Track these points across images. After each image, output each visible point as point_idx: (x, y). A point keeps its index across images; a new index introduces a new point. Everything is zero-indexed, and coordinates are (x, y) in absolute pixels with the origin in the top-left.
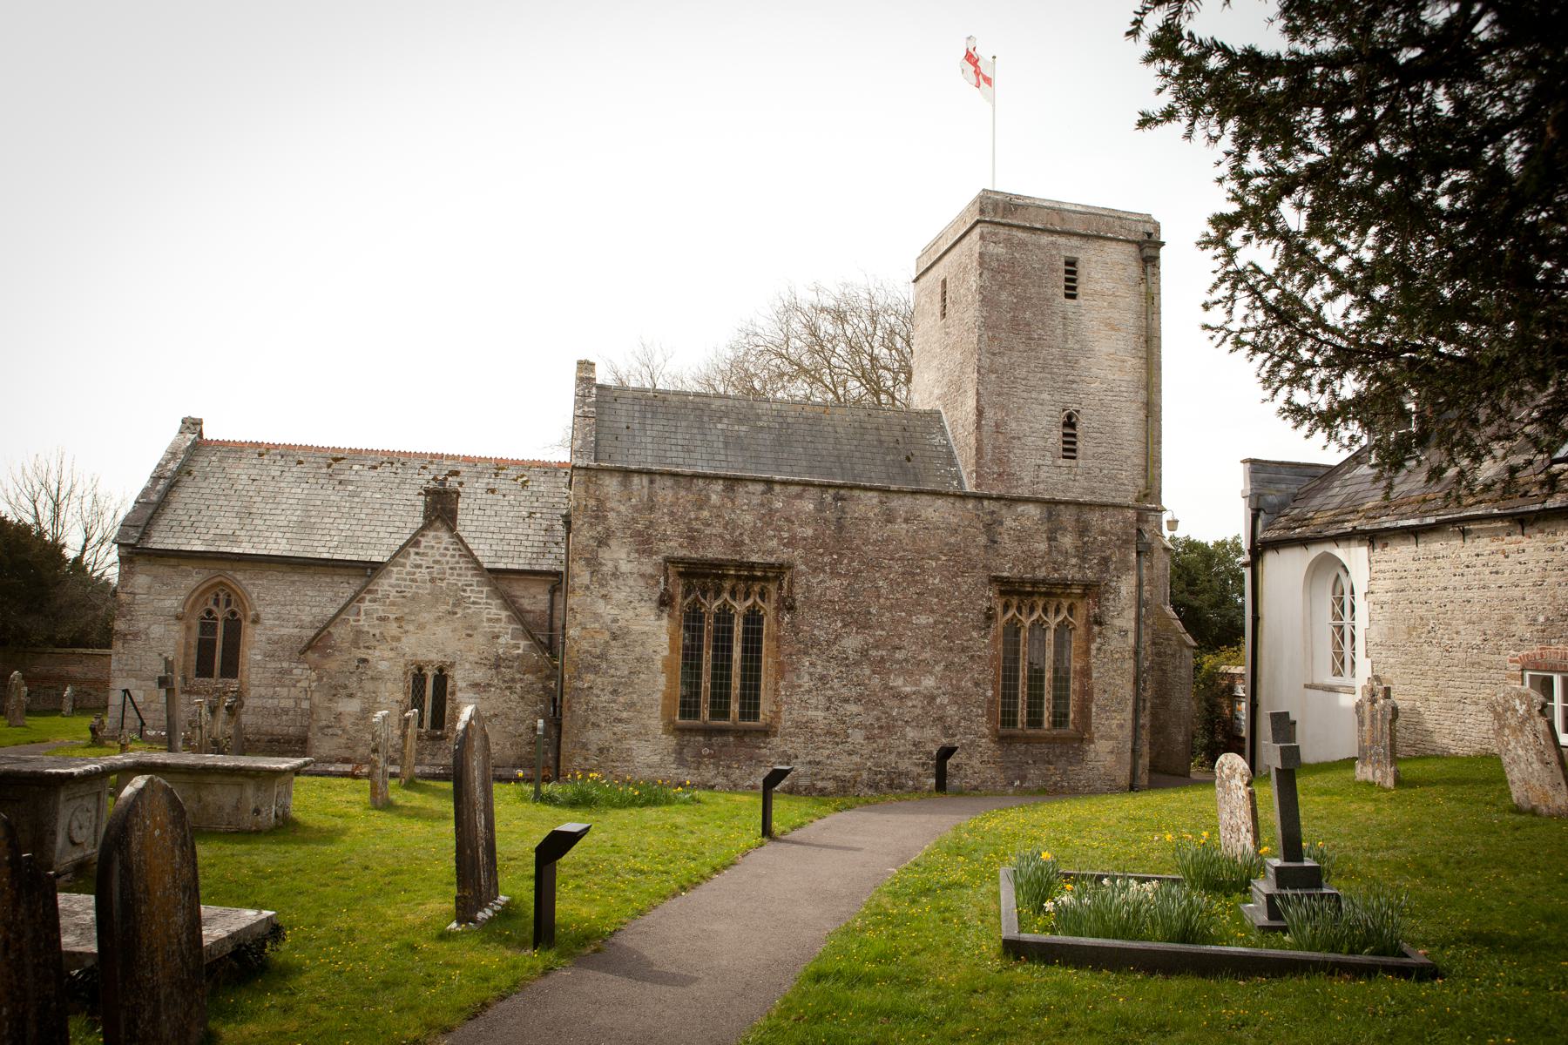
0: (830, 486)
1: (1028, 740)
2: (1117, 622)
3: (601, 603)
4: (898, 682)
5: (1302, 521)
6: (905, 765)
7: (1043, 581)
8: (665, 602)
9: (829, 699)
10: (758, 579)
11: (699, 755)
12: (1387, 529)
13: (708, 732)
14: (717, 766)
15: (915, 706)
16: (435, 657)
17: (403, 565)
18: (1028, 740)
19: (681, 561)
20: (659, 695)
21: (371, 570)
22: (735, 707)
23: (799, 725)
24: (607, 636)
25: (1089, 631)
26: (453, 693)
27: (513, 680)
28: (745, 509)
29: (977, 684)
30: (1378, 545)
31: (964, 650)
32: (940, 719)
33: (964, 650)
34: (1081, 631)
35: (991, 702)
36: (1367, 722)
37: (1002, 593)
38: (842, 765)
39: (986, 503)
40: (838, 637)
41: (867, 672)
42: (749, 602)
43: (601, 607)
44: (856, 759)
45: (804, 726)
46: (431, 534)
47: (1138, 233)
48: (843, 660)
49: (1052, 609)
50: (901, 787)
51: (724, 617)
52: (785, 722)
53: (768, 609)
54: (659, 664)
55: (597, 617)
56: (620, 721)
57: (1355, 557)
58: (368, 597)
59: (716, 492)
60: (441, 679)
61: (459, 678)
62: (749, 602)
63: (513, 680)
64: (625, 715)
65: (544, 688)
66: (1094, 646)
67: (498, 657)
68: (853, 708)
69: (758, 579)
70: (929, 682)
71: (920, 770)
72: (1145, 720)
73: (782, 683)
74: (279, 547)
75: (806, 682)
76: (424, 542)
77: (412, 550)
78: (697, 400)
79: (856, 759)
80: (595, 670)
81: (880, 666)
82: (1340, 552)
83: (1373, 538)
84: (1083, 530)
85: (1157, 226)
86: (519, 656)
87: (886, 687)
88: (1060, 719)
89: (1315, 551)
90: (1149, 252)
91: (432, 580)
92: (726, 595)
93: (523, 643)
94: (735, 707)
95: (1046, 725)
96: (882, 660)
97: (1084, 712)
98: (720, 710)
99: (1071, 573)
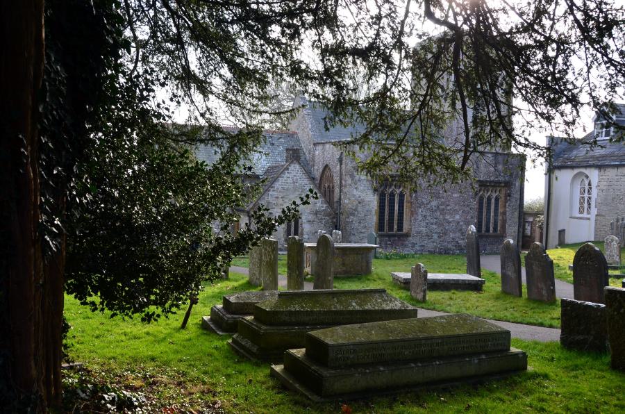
1: (487, 237)
2: (515, 196)
3: (355, 190)
4: (448, 217)
5: (568, 159)
6: (450, 246)
7: (493, 181)
8: (375, 190)
9: (427, 223)
11: (387, 244)
12: (607, 165)
13: (389, 236)
14: (392, 247)
17: (283, 177)
18: (487, 237)
20: (374, 223)
22: (396, 227)
23: (418, 233)
24: (357, 202)
25: (506, 199)
26: (301, 224)
27: (322, 219)
29: (472, 218)
30: (602, 170)
31: (468, 206)
32: (461, 230)
33: (468, 206)
34: (503, 199)
36: (615, 229)
37: (480, 186)
38: (431, 246)
41: (439, 213)
42: (401, 190)
43: (355, 192)
44: (435, 244)
45: (419, 233)
46: (292, 165)
48: (432, 210)
49: (486, 192)
50: (448, 254)
51: (392, 195)
52: (413, 232)
54: (374, 213)
55: (354, 196)
56: (361, 233)
57: (594, 175)
58: (272, 189)
62: (401, 190)
63: (322, 219)
64: (363, 231)
65: (332, 222)
66: (507, 204)
67: (317, 211)
68: (434, 226)
70: (457, 217)
71: (454, 248)
73: (413, 218)
75: (420, 218)
76: (290, 168)
77: (286, 172)
79: (435, 244)
80: (353, 214)
81: (443, 212)
82: (587, 171)
83: (599, 167)
86: (323, 210)
87: (444, 219)
88: (495, 229)
89: (576, 171)
91: (294, 183)
92: (393, 187)
93: (325, 206)
94: (396, 227)
95: (491, 232)
96: (443, 210)
97: (503, 227)
98: (391, 228)
99: (501, 179)
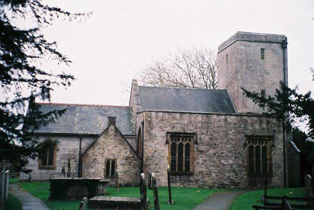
0: (205, 114)
6: (226, 182)
10: (188, 137)
15: (227, 168)
16: (112, 157)
19: (171, 133)
21: (96, 137)
22: (184, 168)
28: (186, 119)
33: (239, 153)
35: (247, 167)
37: (248, 139)
39: (243, 117)
40: (208, 150)
41: (216, 159)
44: (214, 181)
47: (280, 39)
51: (258, 147)
53: (191, 144)
59: (178, 116)
60: (114, 162)
61: (118, 162)
66: (273, 152)
68: (212, 168)
69: (188, 137)
70: (231, 162)
72: (287, 171)
74: (63, 131)
78: (268, 166)
80: (151, 159)
84: (268, 123)
85: (286, 38)
87: (220, 163)
90: (284, 46)
94: (184, 168)
